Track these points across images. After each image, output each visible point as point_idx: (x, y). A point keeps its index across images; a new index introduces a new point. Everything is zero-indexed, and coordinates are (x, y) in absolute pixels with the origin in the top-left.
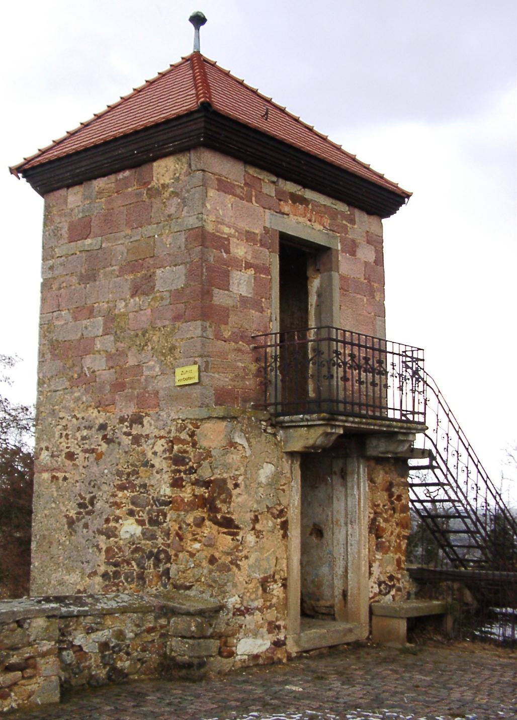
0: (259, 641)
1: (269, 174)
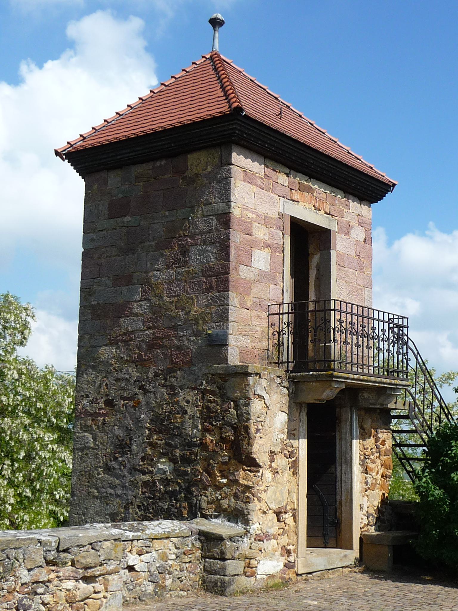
0: (275, 563)
1: (283, 167)
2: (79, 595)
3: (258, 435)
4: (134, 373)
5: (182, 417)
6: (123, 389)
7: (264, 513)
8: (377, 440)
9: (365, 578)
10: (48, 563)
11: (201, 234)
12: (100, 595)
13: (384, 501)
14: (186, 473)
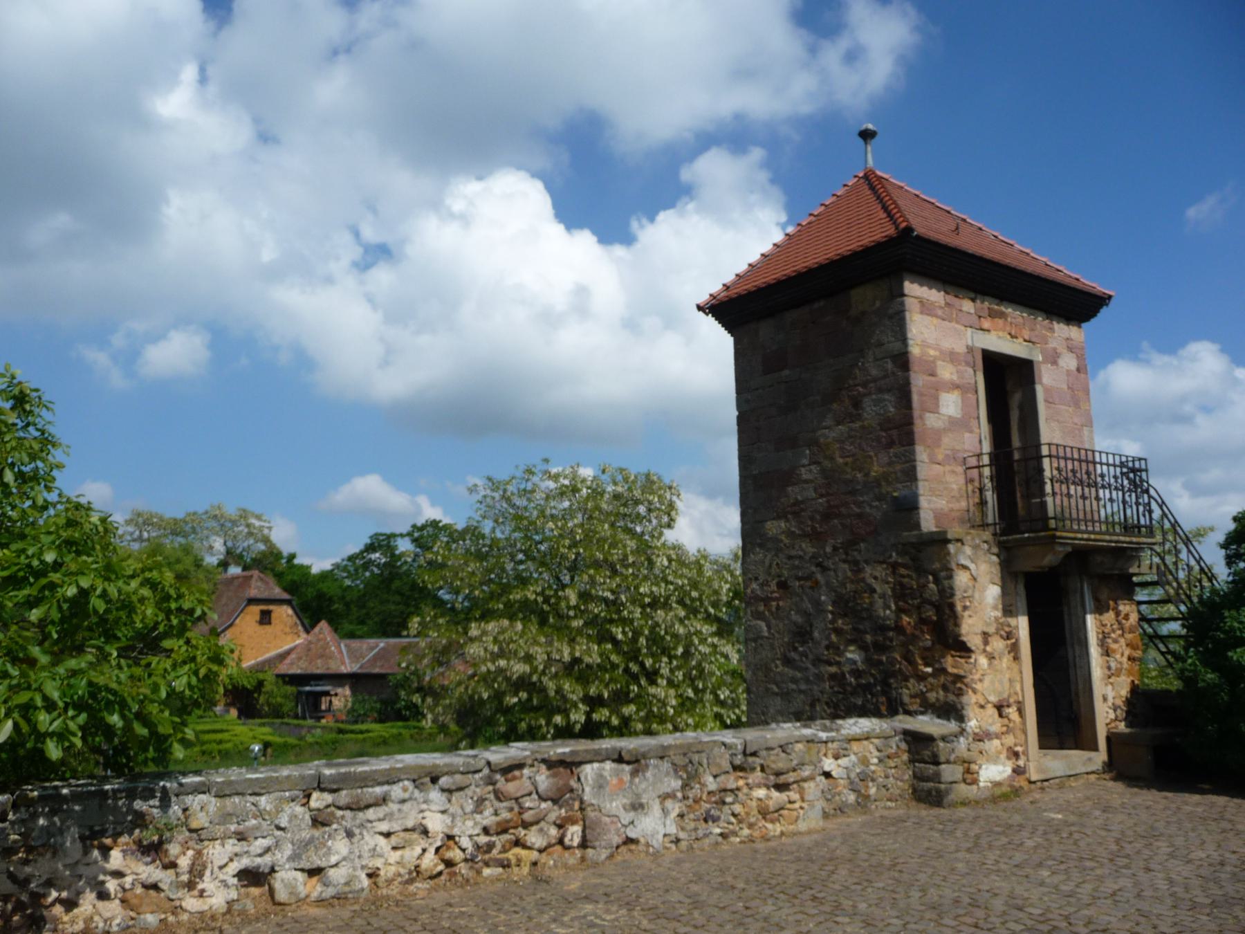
0: (1001, 768)
2: (772, 805)
3: (966, 614)
4: (808, 548)
5: (871, 597)
6: (798, 568)
7: (982, 707)
8: (1118, 614)
9: (1119, 787)
10: (736, 768)
11: (875, 380)
12: (797, 805)
13: (1134, 690)
14: (880, 662)
